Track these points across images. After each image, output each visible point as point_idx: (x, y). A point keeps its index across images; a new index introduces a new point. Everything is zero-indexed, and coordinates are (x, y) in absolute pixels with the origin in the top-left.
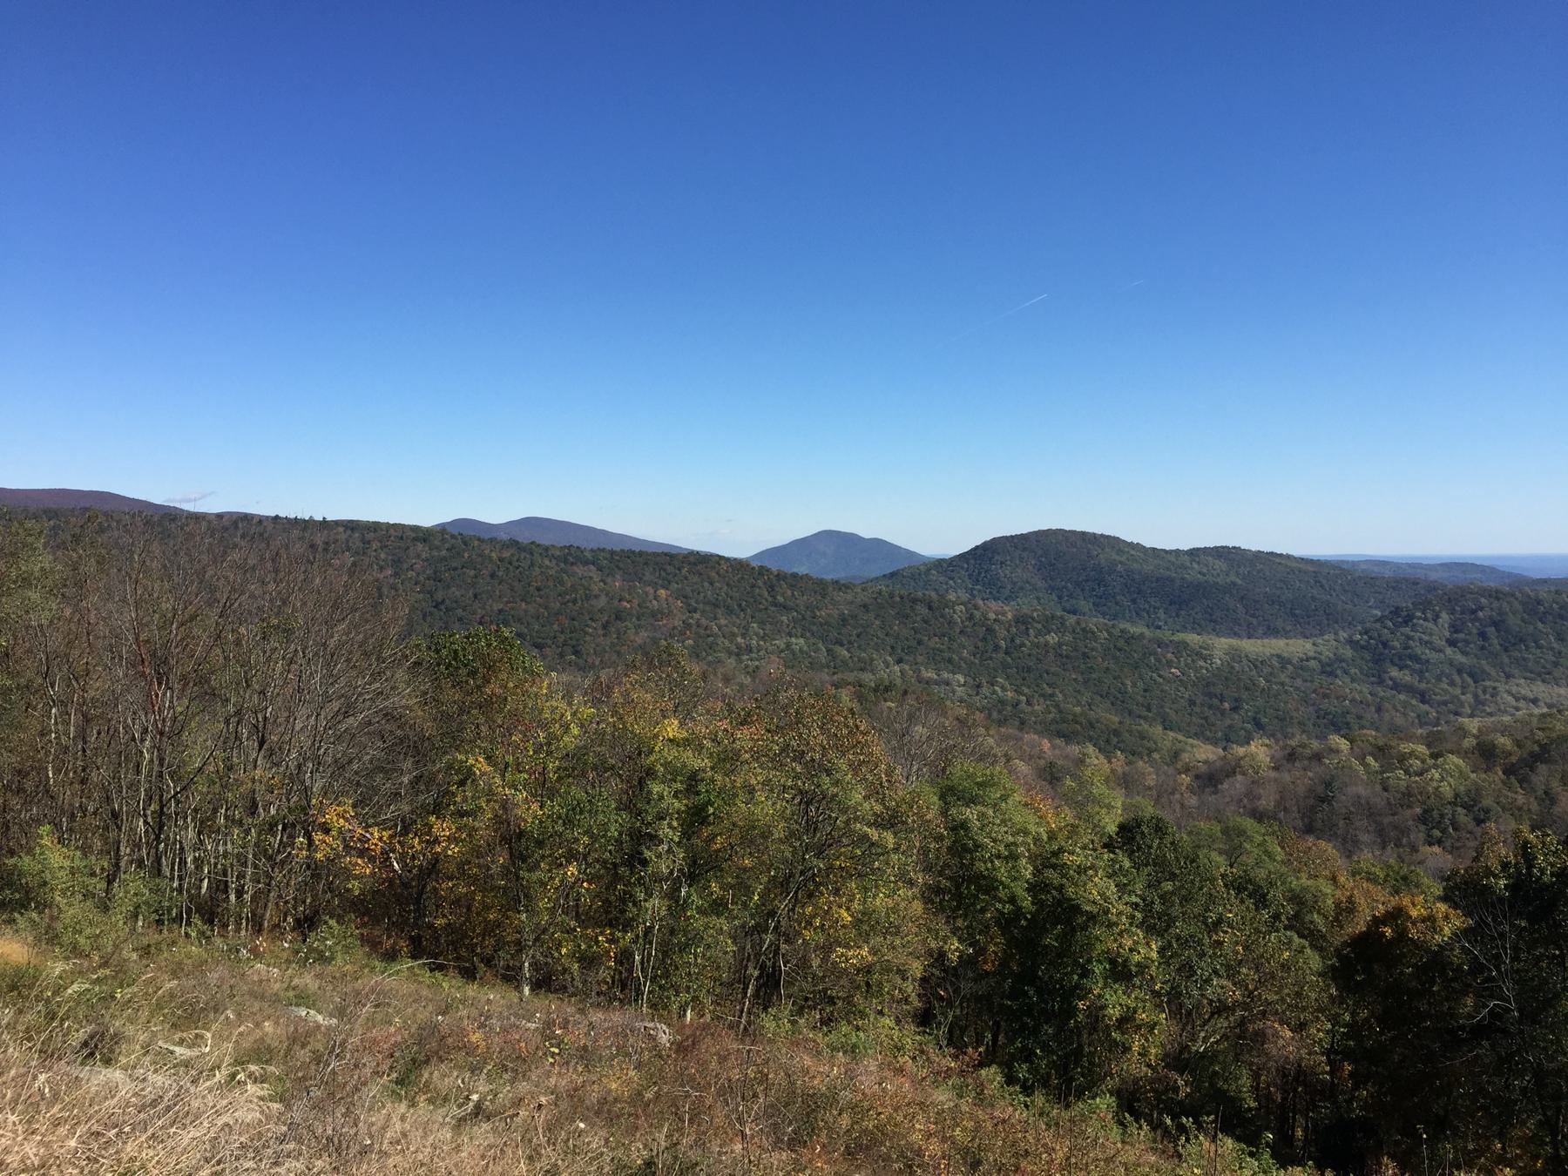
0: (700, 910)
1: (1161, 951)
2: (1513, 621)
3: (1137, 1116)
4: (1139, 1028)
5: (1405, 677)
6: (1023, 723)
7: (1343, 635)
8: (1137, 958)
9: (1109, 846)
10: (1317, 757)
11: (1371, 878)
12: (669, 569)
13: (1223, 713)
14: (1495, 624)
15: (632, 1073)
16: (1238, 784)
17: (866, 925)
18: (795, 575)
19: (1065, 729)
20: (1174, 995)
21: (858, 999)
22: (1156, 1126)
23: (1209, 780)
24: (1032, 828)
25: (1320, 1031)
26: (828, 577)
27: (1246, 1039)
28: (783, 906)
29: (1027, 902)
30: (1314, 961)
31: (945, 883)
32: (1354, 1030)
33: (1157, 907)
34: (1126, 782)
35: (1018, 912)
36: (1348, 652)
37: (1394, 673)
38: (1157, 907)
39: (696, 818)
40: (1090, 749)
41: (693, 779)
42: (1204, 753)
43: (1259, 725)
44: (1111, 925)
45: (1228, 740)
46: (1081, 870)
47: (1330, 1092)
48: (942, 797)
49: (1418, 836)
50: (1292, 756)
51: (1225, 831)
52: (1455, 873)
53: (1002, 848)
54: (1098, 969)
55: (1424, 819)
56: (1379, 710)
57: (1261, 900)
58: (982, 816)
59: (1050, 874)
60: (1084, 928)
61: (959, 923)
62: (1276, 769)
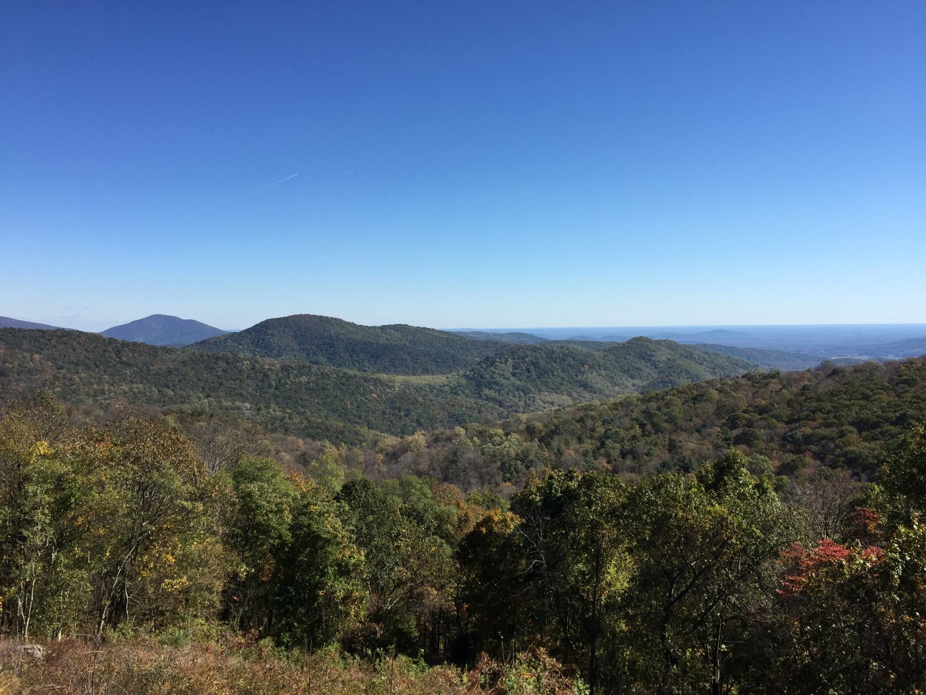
0: (66, 566)
1: (367, 556)
2: (542, 363)
3: (352, 651)
4: (354, 601)
5: (492, 393)
6: (287, 430)
7: (461, 372)
8: (353, 561)
9: (337, 499)
10: (449, 439)
11: (477, 503)
12: (42, 340)
13: (400, 417)
14: (534, 364)
15: (15, 679)
16: (409, 457)
17: (185, 563)
18: (135, 344)
19: (312, 432)
20: (374, 579)
21: (180, 610)
22: (363, 656)
23: (393, 456)
24: (292, 493)
25: (451, 589)
26: (159, 345)
27: (413, 598)
28: (126, 557)
29: (288, 537)
30: (448, 550)
31: (237, 531)
32: (468, 585)
33: (365, 531)
34: (348, 461)
35: (283, 544)
36: (464, 381)
37: (487, 391)
38: (365, 531)
39: (62, 506)
40: (327, 443)
41: (59, 482)
42: (390, 441)
43: (419, 424)
44: (338, 544)
45: (403, 432)
46: (321, 514)
47: (457, 621)
48: (235, 478)
49: (499, 478)
50: (436, 440)
51: (400, 485)
52: (516, 495)
53: (273, 507)
54: (330, 570)
55: (502, 468)
56: (479, 412)
57: (420, 520)
58: (261, 488)
59: (302, 518)
60: (323, 548)
61: (247, 554)
62: (428, 447)
